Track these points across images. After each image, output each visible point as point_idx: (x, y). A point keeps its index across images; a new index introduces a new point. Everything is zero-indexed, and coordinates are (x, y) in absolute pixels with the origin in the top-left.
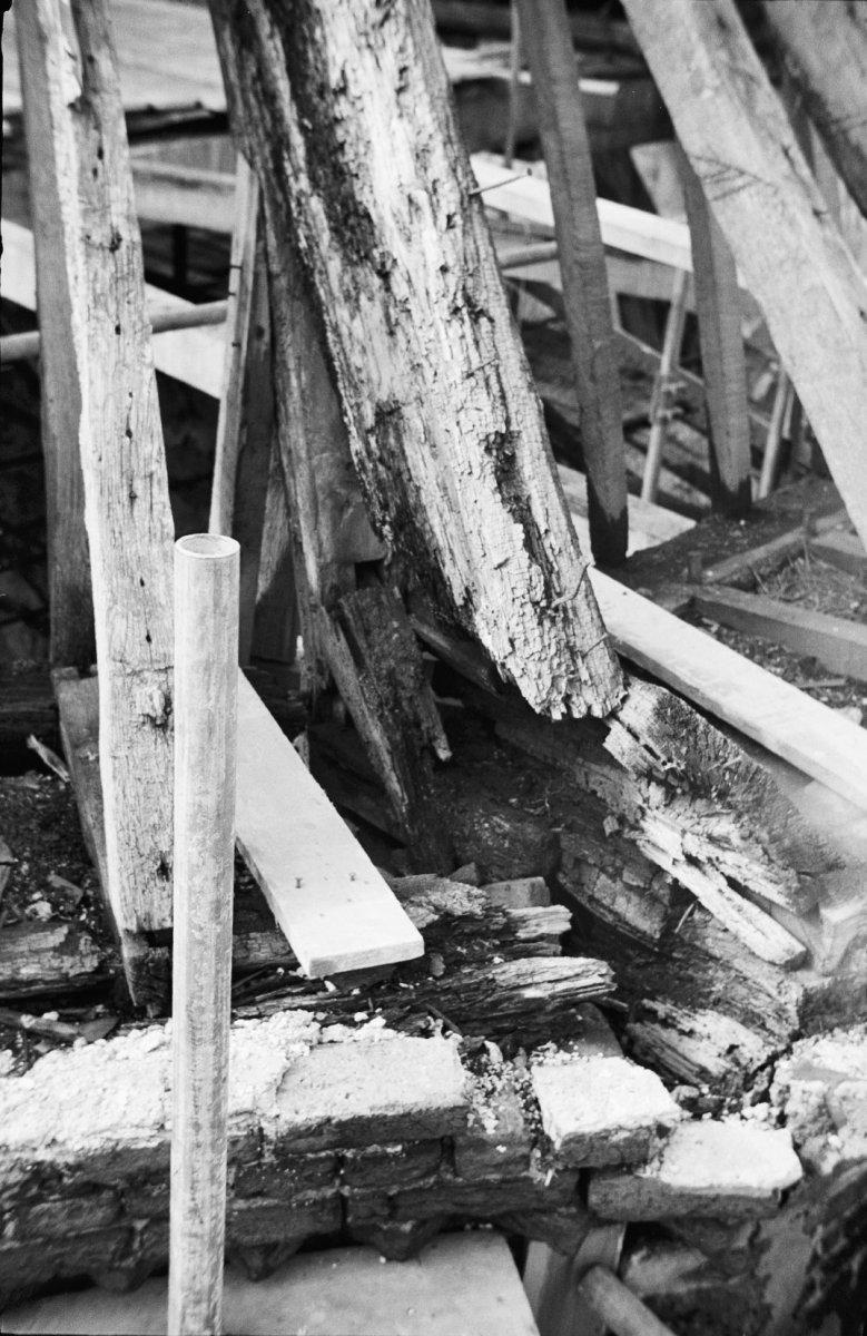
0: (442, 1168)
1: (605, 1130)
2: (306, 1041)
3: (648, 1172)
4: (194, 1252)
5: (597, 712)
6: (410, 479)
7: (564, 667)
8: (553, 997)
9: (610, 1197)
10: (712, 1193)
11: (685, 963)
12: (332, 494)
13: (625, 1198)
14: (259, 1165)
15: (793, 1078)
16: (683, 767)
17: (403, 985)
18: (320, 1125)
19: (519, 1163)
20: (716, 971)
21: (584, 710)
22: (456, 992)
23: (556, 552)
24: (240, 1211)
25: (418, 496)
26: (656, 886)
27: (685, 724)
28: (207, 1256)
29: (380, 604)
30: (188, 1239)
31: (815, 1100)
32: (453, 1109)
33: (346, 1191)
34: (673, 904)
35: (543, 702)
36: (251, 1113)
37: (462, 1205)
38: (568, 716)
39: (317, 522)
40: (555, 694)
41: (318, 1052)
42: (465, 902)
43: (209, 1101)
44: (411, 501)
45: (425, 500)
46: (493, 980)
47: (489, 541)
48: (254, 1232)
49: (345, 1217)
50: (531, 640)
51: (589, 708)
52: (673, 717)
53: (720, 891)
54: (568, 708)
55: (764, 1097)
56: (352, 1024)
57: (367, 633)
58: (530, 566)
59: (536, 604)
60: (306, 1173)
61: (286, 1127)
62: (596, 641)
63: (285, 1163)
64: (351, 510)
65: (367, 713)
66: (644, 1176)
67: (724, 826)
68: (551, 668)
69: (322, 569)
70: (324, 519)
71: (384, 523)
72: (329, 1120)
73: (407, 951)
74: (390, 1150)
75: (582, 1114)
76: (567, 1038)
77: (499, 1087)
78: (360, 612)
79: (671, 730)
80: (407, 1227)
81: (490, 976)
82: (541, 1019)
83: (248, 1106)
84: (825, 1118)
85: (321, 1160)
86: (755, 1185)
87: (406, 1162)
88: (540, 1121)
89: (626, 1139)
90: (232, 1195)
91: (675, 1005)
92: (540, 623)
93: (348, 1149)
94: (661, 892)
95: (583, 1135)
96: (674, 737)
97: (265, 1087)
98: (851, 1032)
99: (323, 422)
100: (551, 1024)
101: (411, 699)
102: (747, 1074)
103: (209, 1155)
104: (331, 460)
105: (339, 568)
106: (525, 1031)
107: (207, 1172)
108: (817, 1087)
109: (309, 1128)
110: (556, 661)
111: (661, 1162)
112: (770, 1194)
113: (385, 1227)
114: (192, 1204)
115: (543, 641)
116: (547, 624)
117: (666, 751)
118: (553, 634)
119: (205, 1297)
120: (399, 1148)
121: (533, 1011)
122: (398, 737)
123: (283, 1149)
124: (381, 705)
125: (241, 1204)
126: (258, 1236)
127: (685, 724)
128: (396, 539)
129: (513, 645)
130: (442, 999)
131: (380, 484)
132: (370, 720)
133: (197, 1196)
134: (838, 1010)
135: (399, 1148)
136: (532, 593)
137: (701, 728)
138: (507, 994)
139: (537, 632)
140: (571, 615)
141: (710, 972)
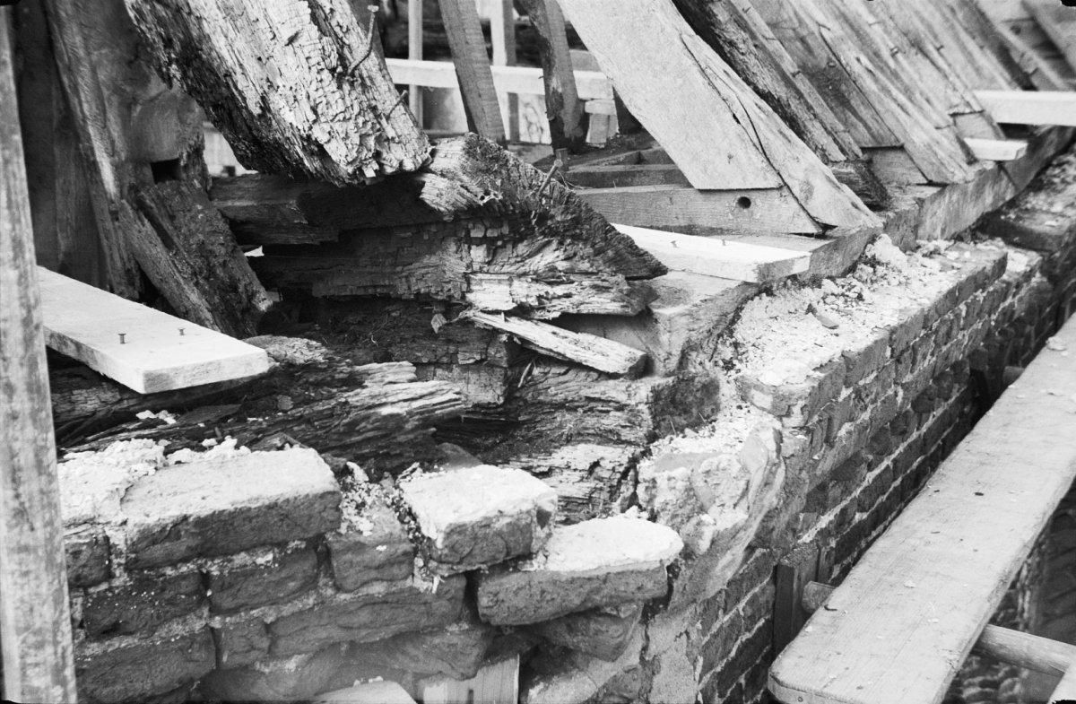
0: (321, 584)
1: (486, 518)
2: (149, 462)
3: (535, 565)
4: (26, 574)
5: (409, 166)
6: (190, 13)
7: (369, 125)
8: (410, 413)
9: (501, 596)
10: (602, 573)
11: (532, 422)
12: (117, 90)
13: (516, 593)
14: (110, 589)
15: (656, 471)
16: (500, 197)
17: (251, 419)
18: (175, 525)
19: (401, 563)
20: (564, 416)
21: (396, 164)
22: (309, 421)
23: (344, 30)
24: (94, 657)
25: (200, 28)
26: (492, 351)
27: (496, 159)
28: (45, 578)
29: (181, 193)
30: (16, 557)
31: (681, 485)
32: (323, 496)
33: (217, 622)
34: (511, 366)
35: (354, 161)
36: (91, 521)
37: (348, 628)
38: (380, 172)
39: (105, 120)
40: (365, 152)
41: (163, 472)
42: (306, 351)
43: (20, 350)
44: (195, 33)
45: (207, 29)
46: (346, 403)
47: (276, 19)
48: (114, 682)
49: (219, 653)
50: (333, 102)
51: (401, 163)
52: (483, 154)
53: (554, 333)
54: (381, 165)
55: (633, 500)
56: (203, 449)
57: (172, 218)
58: (320, 39)
59: (333, 71)
60: (167, 595)
61: (136, 530)
62: (395, 102)
63: (143, 584)
64: (139, 108)
65: (182, 281)
66: (532, 569)
67: (553, 256)
68: (356, 125)
69: (117, 168)
70: (112, 116)
71: (170, 63)
72: (185, 518)
73: (249, 364)
74: (260, 561)
75: (461, 507)
76: (431, 462)
77: (369, 501)
78: (161, 201)
79: (482, 165)
80: (291, 665)
81: (343, 400)
82: (401, 438)
83: (87, 511)
84: (693, 500)
85: (183, 577)
86: (642, 558)
87: (280, 571)
88: (418, 529)
89: (508, 524)
90: (82, 634)
91: (530, 457)
92: (340, 87)
93: (213, 558)
94: (498, 355)
95: (464, 525)
96: (487, 171)
97: (106, 494)
98: (701, 432)
99: (98, 18)
100: (412, 444)
101: (224, 265)
102: (611, 487)
103: (30, 432)
104: (111, 56)
105: (135, 168)
106: (387, 455)
107: (31, 455)
108: (680, 472)
109: (164, 529)
110: (361, 120)
111: (546, 557)
112: (659, 565)
113: (267, 670)
114: (16, 504)
115: (345, 103)
116: (346, 87)
117: (481, 184)
118: (354, 97)
119: (49, 637)
120: (270, 557)
121: (392, 431)
122: (216, 299)
123: (136, 560)
124: (194, 274)
125: (94, 648)
126: (119, 687)
127: (496, 159)
128: (185, 76)
129: (315, 112)
130: (296, 428)
131: (160, 21)
132: (186, 287)
133: (21, 490)
134: (686, 412)
135: (270, 557)
136: (327, 61)
137: (511, 162)
138: (363, 413)
139: (337, 95)
140: (368, 83)
141: (559, 419)
